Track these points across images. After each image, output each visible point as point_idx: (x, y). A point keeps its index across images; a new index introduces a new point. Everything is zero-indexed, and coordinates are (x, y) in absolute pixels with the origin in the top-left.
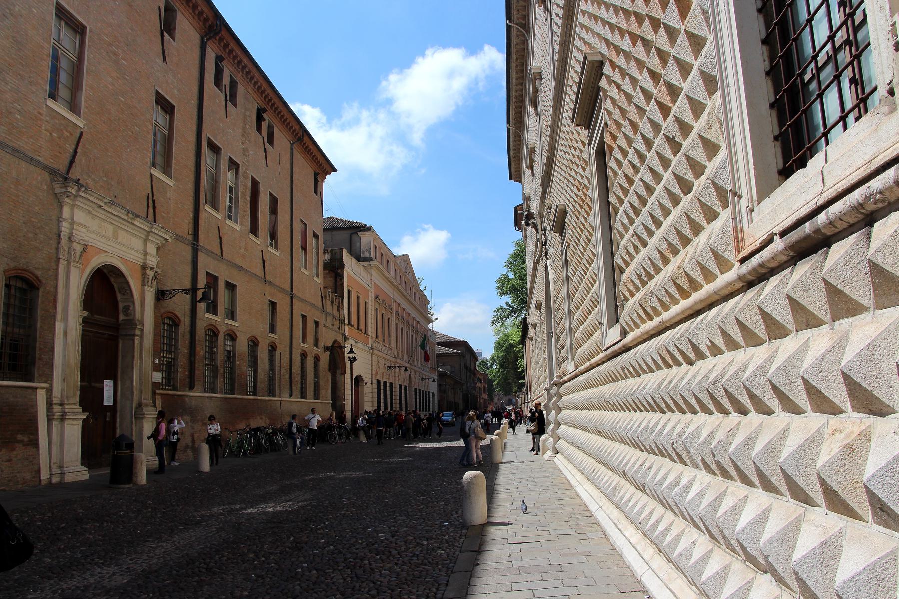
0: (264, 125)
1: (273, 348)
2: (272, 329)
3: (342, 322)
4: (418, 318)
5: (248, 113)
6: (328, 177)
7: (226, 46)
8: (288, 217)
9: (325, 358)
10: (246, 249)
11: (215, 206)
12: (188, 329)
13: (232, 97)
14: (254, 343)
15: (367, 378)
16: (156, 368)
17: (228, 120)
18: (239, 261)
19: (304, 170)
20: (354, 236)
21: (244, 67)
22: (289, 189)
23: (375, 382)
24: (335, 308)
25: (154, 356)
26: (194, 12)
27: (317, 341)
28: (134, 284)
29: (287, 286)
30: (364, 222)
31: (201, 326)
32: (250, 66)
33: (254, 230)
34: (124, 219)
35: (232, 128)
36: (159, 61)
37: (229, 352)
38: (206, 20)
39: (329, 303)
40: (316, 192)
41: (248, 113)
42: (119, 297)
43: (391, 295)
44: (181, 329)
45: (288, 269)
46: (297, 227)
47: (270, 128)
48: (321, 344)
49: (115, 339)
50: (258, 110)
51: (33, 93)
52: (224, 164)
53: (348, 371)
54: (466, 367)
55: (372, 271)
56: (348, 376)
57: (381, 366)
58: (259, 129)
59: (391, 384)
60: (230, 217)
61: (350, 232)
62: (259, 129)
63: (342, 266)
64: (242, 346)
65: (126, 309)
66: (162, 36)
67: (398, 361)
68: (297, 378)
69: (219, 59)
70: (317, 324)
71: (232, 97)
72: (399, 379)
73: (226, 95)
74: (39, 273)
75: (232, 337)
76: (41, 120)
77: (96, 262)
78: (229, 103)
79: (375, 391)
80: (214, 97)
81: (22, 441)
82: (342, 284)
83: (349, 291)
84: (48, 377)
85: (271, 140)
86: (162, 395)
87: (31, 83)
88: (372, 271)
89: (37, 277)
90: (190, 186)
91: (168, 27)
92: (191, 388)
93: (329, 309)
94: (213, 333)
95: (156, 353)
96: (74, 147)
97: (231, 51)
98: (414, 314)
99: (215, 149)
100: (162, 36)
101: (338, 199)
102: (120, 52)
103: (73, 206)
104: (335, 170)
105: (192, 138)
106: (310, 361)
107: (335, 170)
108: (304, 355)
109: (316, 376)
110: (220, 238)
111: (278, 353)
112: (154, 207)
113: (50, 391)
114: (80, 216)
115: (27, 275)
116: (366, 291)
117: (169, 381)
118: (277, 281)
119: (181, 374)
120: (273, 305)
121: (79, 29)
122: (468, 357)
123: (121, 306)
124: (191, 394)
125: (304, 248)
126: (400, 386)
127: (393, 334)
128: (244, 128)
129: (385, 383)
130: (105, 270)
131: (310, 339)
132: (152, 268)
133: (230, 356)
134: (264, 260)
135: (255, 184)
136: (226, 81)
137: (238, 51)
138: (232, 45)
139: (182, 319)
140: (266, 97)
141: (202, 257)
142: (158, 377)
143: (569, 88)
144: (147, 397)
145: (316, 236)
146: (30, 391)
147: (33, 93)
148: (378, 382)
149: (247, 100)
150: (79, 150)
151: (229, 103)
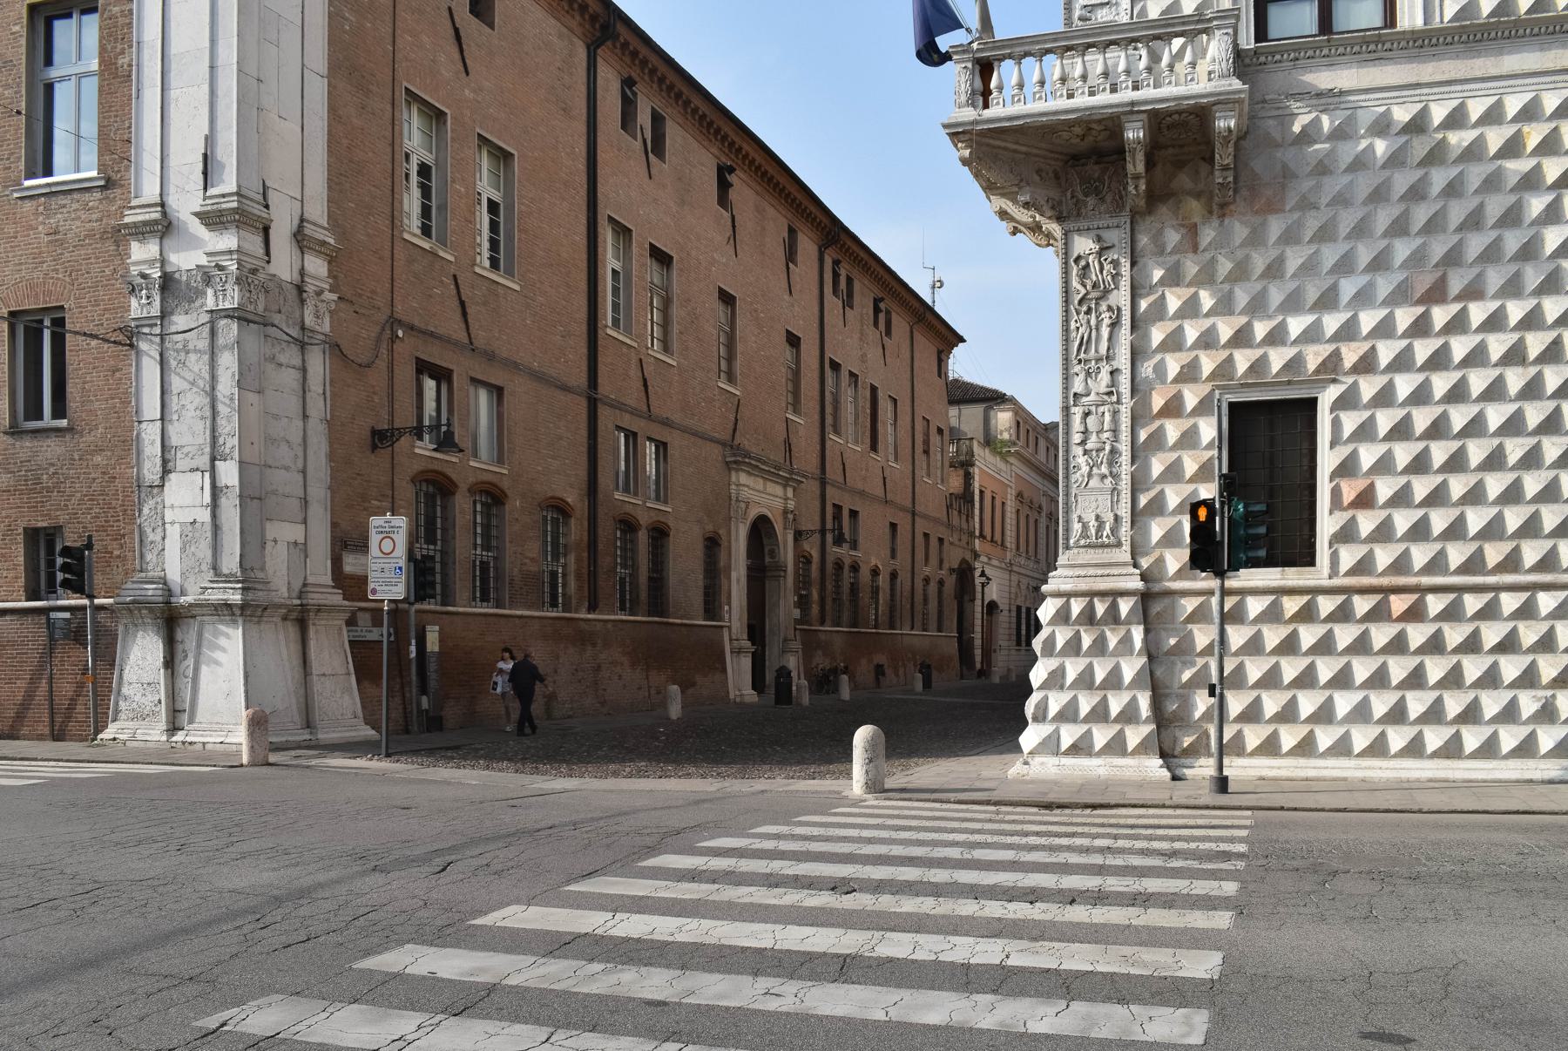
3: (972, 534)
8: (909, 419)
9: (950, 582)
19: (926, 348)
27: (941, 561)
31: (830, 559)
33: (874, 447)
36: (786, 297)
42: (765, 541)
48: (946, 565)
53: (979, 596)
57: (1023, 587)
58: (876, 324)
64: (865, 573)
65: (772, 553)
69: (628, 83)
70: (941, 540)
77: (753, 513)
83: (981, 492)
92: (822, 623)
94: (839, 565)
101: (963, 365)
104: (962, 340)
107: (962, 340)
108: (927, 580)
120: (893, 526)
125: (926, 452)
131: (934, 560)
133: (854, 589)
141: (829, 490)
148: (1019, 608)
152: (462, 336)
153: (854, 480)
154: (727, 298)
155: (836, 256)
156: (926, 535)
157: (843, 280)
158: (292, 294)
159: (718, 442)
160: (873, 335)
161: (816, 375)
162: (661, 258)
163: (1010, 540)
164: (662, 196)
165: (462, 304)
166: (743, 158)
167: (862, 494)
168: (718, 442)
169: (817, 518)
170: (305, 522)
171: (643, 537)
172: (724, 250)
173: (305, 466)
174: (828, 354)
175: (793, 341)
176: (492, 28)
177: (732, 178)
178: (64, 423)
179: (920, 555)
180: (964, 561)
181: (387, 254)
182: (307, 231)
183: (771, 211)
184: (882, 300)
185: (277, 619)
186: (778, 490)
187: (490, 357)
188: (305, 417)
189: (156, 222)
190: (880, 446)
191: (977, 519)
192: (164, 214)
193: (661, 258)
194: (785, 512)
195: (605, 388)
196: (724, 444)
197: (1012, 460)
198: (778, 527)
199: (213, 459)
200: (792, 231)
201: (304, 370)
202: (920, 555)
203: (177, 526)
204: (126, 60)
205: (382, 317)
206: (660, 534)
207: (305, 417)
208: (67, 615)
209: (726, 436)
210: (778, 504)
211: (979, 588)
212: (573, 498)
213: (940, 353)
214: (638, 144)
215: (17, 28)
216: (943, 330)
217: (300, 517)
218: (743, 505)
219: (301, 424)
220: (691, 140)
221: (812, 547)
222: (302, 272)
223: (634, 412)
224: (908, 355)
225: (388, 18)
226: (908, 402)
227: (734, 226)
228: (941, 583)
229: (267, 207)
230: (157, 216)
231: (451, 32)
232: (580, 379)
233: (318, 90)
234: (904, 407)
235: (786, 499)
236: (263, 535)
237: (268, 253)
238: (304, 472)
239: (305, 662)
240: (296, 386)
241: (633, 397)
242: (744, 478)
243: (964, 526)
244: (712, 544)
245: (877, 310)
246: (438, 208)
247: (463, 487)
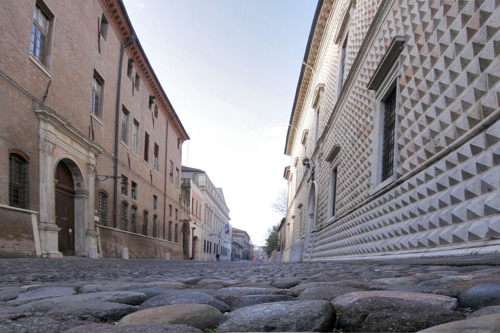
0: (153, 106)
1: (155, 217)
2: (155, 208)
3: (189, 212)
5: (145, 97)
6: (185, 142)
7: (135, 53)
8: (164, 157)
9: (181, 225)
10: (142, 168)
12: (112, 200)
14: (146, 213)
15: (199, 238)
16: (96, 215)
17: (134, 97)
18: (139, 173)
19: (173, 136)
21: (145, 69)
22: (165, 144)
24: (186, 205)
25: (95, 209)
28: (83, 170)
29: (163, 190)
32: (148, 69)
34: (77, 136)
35: (137, 101)
36: (97, 51)
37: (133, 215)
38: (125, 34)
39: (183, 202)
40: (178, 148)
41: (145, 97)
42: (74, 178)
44: (109, 199)
45: (163, 182)
46: (169, 163)
47: (156, 107)
48: (178, 219)
49: (72, 198)
51: (21, 48)
53: (191, 233)
54: (245, 241)
56: (191, 235)
57: (207, 234)
58: (150, 107)
62: (150, 107)
63: (190, 187)
64: (140, 212)
65: (79, 185)
66: (99, 37)
68: (167, 232)
69: (131, 61)
70: (177, 210)
71: (136, 85)
73: (133, 83)
74: (28, 154)
75: (134, 208)
76: (26, 66)
77: (62, 155)
78: (135, 89)
80: (127, 83)
81: (25, 237)
83: (193, 199)
84: (38, 209)
85: (156, 114)
86: (100, 227)
87: (19, 41)
89: (27, 156)
90: (113, 128)
91: (102, 32)
92: (115, 227)
93: (183, 205)
94: (125, 204)
95: (96, 207)
96: (46, 88)
97: (138, 57)
99: (126, 112)
100: (99, 37)
101: (191, 156)
102: (74, 38)
104: (189, 138)
105: (114, 101)
106: (173, 226)
107: (189, 138)
108: (170, 223)
110: (129, 159)
111: (158, 219)
112: (93, 135)
113: (38, 216)
115: (20, 153)
117: (104, 221)
118: (158, 187)
119: (109, 219)
120: (155, 197)
121: (48, 15)
122: (246, 238)
123: (75, 182)
125: (171, 175)
128: (142, 105)
129: (208, 242)
130: (66, 163)
132: (93, 165)
133: (134, 216)
134: (151, 176)
135: (147, 136)
137: (142, 58)
138: (139, 54)
139: (109, 194)
141: (119, 168)
142: (97, 219)
143: (391, 14)
144: (92, 227)
146: (27, 215)
147: (21, 48)
148: (205, 240)
149: (144, 92)
150: (49, 90)
151: (135, 89)
156: (170, 206)
159: (28, 96)
161: (113, 115)
162: (137, 123)
163: (202, 218)
167: (139, 177)
168: (28, 96)
174: (121, 103)
179: (167, 212)
186: (84, 151)
191: (191, 207)
196: (34, 100)
197: (204, 192)
202: (167, 212)
209: (39, 95)
211: (191, 230)
216: (181, 129)
228: (176, 225)
234: (161, 151)
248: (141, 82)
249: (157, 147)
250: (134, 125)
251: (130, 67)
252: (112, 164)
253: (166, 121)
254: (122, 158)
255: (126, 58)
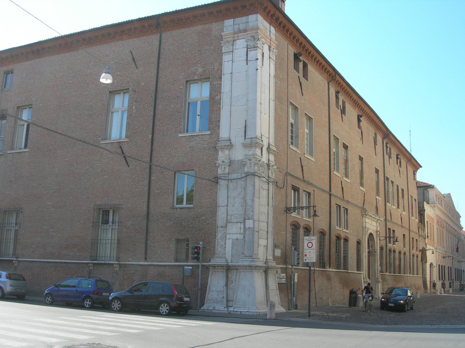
2: (404, 247)
4: (456, 228)
9: (420, 254)
11: (338, 171)
13: (343, 111)
15: (434, 265)
20: (425, 191)
21: (328, 72)
23: (438, 266)
26: (276, 22)
27: (417, 248)
30: (430, 183)
31: (388, 248)
33: (398, 207)
36: (375, 156)
43: (443, 218)
50: (358, 116)
52: (340, 145)
55: (436, 209)
57: (440, 257)
59: (444, 266)
60: (292, 143)
61: (423, 189)
63: (424, 210)
67: (448, 254)
68: (397, 268)
69: (337, 93)
70: (417, 240)
72: (447, 263)
79: (438, 270)
82: (424, 219)
85: (305, 75)
88: (436, 209)
98: (454, 226)
99: (337, 139)
101: (422, 176)
103: (365, 217)
104: (421, 167)
107: (421, 167)
109: (417, 264)
114: (367, 220)
116: (433, 219)
120: (404, 235)
124: (330, 270)
126: (448, 267)
127: (445, 240)
129: (442, 266)
131: (415, 248)
136: (341, 103)
140: (330, 74)
145: (415, 200)
148: (439, 265)
152: (302, 177)
153: (394, 220)
154: (361, 159)
155: (387, 141)
157: (388, 149)
158: (266, 167)
160: (397, 167)
162: (345, 147)
164: (346, 127)
165: (302, 166)
166: (366, 113)
169: (384, 233)
170: (267, 239)
171: (342, 241)
172: (361, 144)
173: (268, 221)
174: (386, 175)
175: (377, 171)
176: (307, 80)
177: (361, 119)
178: (191, 206)
180: (423, 248)
181: (286, 152)
182: (271, 147)
183: (370, 128)
184: (399, 155)
185: (262, 271)
186: (374, 223)
187: (309, 183)
188: (268, 205)
189: (229, 146)
190: (400, 206)
192: (231, 143)
193: (345, 147)
194: (377, 232)
195: (333, 192)
198: (375, 237)
199: (245, 219)
200: (375, 134)
201: (268, 190)
203: (231, 240)
204: (219, 97)
205: (284, 172)
206: (346, 240)
207: (268, 205)
208: (191, 268)
210: (375, 229)
212: (326, 229)
213: (414, 172)
214: (339, 111)
215: (182, 87)
217: (266, 238)
218: (367, 229)
219: (267, 207)
220: (351, 108)
221: (383, 243)
222: (269, 160)
223: (339, 198)
224: (406, 174)
225: (286, 82)
226: (407, 191)
227: (362, 134)
229: (262, 141)
230: (228, 144)
231: (299, 83)
232: (328, 189)
233: (272, 104)
234: (406, 192)
235: (377, 227)
236: (258, 244)
237: (262, 155)
238: (268, 223)
239: (266, 285)
240: (266, 195)
241: (340, 194)
242: (367, 220)
243: (423, 235)
244: (359, 243)
245: (397, 158)
246: (295, 137)
247: (302, 226)
248: (310, 68)
249: (403, 190)
250: (343, 149)
251: (337, 98)
252: (408, 232)
253: (405, 164)
254: (336, 191)
255: (333, 91)
